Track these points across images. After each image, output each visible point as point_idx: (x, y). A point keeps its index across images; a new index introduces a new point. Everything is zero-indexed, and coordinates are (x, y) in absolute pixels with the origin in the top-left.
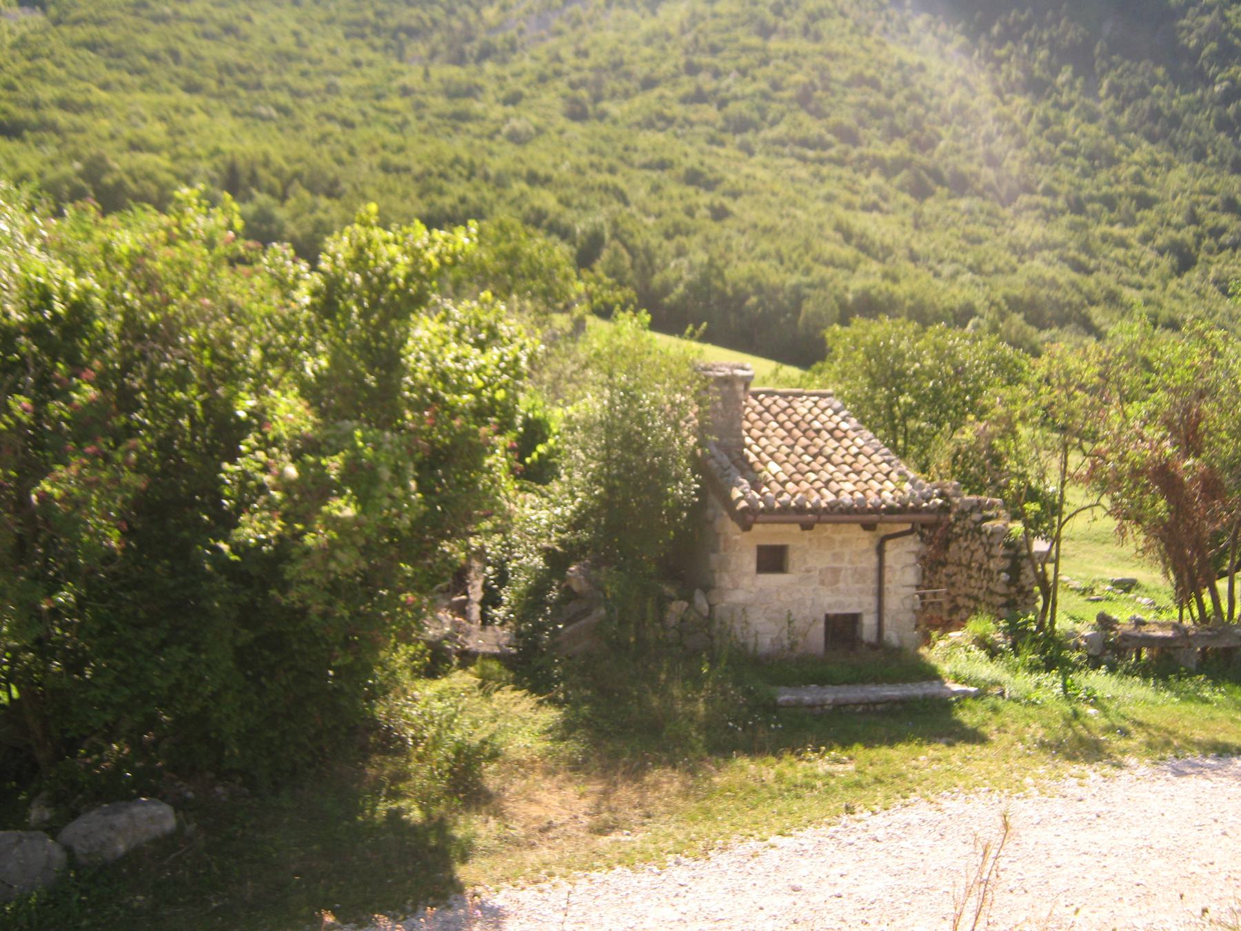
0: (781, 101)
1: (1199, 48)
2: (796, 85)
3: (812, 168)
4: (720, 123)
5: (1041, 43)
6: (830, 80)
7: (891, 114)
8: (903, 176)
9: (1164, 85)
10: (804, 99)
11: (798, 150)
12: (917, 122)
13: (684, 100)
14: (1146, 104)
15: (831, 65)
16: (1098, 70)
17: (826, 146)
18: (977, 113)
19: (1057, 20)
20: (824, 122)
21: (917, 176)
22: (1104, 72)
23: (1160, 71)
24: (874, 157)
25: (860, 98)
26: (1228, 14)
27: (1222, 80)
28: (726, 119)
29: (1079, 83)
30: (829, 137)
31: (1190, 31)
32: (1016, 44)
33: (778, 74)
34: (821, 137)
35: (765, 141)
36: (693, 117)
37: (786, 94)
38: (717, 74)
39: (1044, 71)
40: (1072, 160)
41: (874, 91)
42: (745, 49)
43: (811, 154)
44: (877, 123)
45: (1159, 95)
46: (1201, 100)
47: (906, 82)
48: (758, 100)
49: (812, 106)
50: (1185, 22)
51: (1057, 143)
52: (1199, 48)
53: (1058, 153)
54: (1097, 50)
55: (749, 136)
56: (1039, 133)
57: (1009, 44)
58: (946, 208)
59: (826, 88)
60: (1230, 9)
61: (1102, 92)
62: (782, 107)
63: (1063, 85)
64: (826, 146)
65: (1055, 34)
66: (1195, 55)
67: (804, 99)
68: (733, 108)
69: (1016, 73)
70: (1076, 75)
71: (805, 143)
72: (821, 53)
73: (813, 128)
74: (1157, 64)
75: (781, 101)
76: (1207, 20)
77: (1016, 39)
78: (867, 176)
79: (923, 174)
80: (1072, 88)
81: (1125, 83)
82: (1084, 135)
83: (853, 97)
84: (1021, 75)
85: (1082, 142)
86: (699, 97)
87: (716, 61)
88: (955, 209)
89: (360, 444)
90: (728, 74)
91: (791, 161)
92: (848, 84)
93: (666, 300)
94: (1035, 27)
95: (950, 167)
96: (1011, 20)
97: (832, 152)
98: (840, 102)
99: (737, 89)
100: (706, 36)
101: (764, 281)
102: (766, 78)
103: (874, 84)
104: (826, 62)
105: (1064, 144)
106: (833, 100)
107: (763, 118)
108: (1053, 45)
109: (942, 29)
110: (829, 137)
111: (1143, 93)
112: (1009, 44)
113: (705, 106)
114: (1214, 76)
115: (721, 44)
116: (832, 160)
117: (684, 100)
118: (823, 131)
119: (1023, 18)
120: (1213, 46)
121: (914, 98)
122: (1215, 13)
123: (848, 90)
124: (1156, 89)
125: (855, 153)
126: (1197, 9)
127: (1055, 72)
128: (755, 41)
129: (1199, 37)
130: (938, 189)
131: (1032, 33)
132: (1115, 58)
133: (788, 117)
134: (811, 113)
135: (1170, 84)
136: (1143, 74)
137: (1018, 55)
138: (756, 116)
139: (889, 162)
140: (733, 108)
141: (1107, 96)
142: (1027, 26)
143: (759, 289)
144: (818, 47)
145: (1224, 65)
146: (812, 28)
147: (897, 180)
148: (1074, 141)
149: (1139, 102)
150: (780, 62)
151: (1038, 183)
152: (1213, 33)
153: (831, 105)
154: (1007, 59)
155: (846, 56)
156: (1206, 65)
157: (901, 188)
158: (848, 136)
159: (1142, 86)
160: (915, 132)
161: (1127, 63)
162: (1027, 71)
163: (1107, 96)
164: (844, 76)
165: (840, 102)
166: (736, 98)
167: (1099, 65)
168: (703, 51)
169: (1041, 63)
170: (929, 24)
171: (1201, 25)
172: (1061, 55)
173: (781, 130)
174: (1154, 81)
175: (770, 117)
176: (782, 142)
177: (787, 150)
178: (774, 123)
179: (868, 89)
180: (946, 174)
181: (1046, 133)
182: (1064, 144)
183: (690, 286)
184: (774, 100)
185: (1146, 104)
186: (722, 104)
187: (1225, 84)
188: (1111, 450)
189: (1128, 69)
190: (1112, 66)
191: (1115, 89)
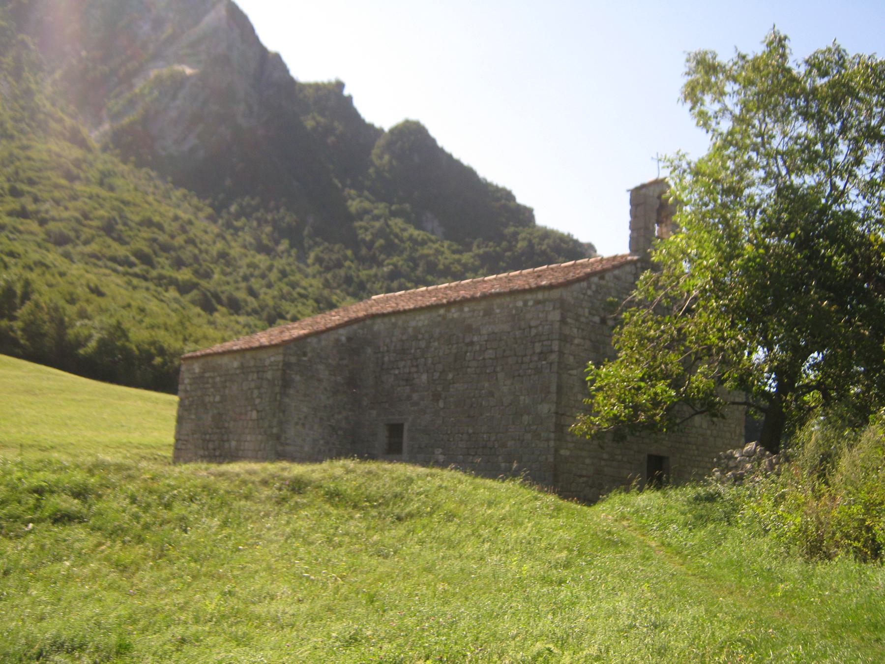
0: (90, 227)
1: (373, 242)
2: (101, 218)
3: (126, 279)
4: (43, 236)
5: (266, 221)
6: (127, 218)
7: (174, 249)
8: (194, 294)
9: (352, 261)
10: (109, 229)
11: (110, 264)
12: (196, 258)
13: (10, 214)
14: (342, 272)
15: (126, 209)
16: (306, 245)
17: (131, 265)
18: (235, 259)
19: (277, 208)
20: (128, 247)
21: (205, 295)
22: (310, 248)
23: (349, 253)
24: (171, 277)
25: (150, 235)
26: (390, 223)
27: (388, 264)
28: (48, 233)
29: (294, 252)
30: (133, 259)
31: (366, 230)
32: (248, 220)
33: (86, 208)
34: (127, 257)
35: (83, 254)
36: (21, 228)
37: (95, 223)
38: (36, 200)
39: (270, 241)
40: (305, 301)
41: (160, 233)
42: (57, 186)
43: (120, 268)
44: (165, 255)
45: (350, 268)
46: (376, 276)
47: (184, 230)
48: (74, 224)
49: (115, 235)
50: (362, 223)
51: (294, 288)
52: (373, 242)
53: (295, 295)
54: (306, 233)
55: (69, 248)
56: (280, 280)
57: (243, 219)
58: (231, 321)
59: (125, 224)
60: (390, 220)
61: (310, 261)
62: (93, 232)
63: (283, 252)
64: (131, 265)
65: (276, 217)
66: (370, 245)
67: (109, 229)
68: (51, 226)
69: (249, 239)
70: (292, 246)
71: (113, 259)
72: (116, 199)
73: (122, 251)
74: (347, 248)
75: (90, 227)
76: (377, 224)
77: (248, 216)
78: (167, 290)
79: (209, 294)
80: (290, 255)
81: (326, 257)
82: (311, 286)
83: (146, 233)
84: (253, 241)
85: (310, 290)
86: (23, 214)
87: (34, 190)
88: (238, 322)
89: (642, 277)
90: (45, 201)
91: (107, 271)
92: (141, 224)
93: (81, 351)
94: (262, 210)
95: (226, 294)
96: (244, 203)
97: (137, 270)
98: (136, 235)
99: (54, 213)
100: (24, 171)
101: (166, 346)
102: (76, 209)
103: (160, 227)
104: (122, 206)
105: (299, 290)
106: (131, 233)
107: (78, 238)
108: (275, 224)
109: (195, 201)
110: (133, 259)
111: (339, 265)
112: (243, 219)
113: (29, 221)
114: (383, 261)
115: (37, 180)
116: (136, 275)
117: (10, 214)
118: (129, 254)
119: (253, 203)
120: (381, 242)
121: (191, 241)
122: (382, 221)
123: (140, 228)
124: (347, 263)
125: (154, 273)
126: (370, 217)
127: (277, 243)
128: (64, 182)
129: (372, 234)
130: (219, 307)
131: (259, 214)
132: (318, 239)
133: (97, 240)
134: (114, 239)
135: (356, 261)
136: (338, 252)
137: (250, 228)
138: (72, 234)
139: (181, 283)
140: (51, 226)
141: (314, 264)
142: (256, 209)
143: (162, 352)
144: (112, 194)
145: (389, 255)
146: (107, 181)
147: (189, 297)
148: (305, 289)
149: (337, 271)
150: (87, 200)
151: (288, 313)
152: (380, 233)
153: (130, 236)
154: (242, 229)
155: (135, 205)
156: (377, 253)
157: (193, 302)
158: (145, 259)
159: (338, 260)
160: (196, 266)
161: (326, 244)
162: (258, 239)
163: (314, 264)
164: (137, 219)
165: (136, 235)
166: (53, 219)
167: (307, 243)
168: (22, 182)
169: (267, 235)
170: (185, 196)
171: (373, 227)
172: (280, 232)
173: (94, 247)
174: (346, 258)
175: (83, 237)
176: (94, 256)
177: (100, 263)
178: (86, 243)
179: (156, 230)
180: (224, 297)
181: (286, 280)
182: (299, 290)
183: (102, 342)
184: (85, 226)
185: (342, 272)
186: (43, 222)
187: (391, 267)
188: (313, 529)
189: (327, 248)
190: (317, 244)
191: (319, 260)
